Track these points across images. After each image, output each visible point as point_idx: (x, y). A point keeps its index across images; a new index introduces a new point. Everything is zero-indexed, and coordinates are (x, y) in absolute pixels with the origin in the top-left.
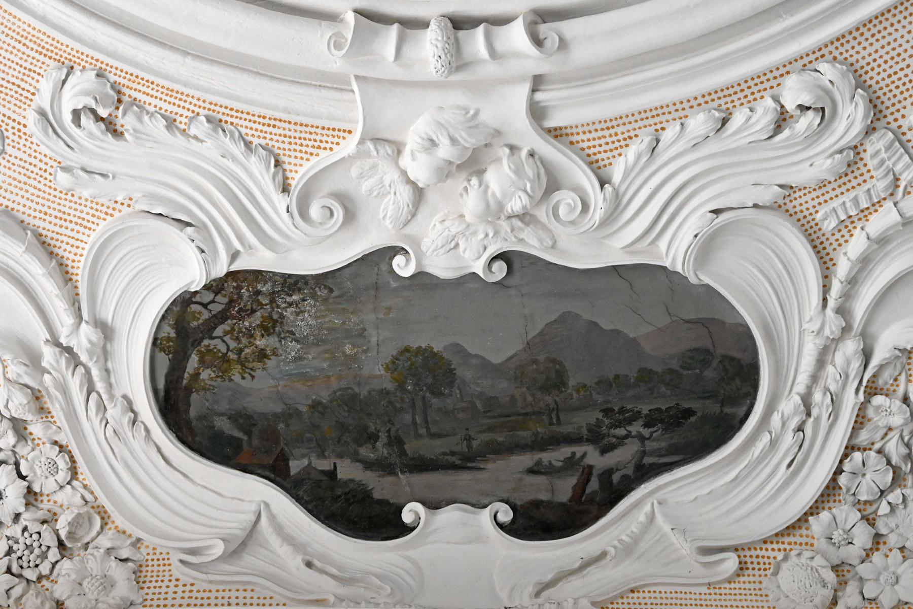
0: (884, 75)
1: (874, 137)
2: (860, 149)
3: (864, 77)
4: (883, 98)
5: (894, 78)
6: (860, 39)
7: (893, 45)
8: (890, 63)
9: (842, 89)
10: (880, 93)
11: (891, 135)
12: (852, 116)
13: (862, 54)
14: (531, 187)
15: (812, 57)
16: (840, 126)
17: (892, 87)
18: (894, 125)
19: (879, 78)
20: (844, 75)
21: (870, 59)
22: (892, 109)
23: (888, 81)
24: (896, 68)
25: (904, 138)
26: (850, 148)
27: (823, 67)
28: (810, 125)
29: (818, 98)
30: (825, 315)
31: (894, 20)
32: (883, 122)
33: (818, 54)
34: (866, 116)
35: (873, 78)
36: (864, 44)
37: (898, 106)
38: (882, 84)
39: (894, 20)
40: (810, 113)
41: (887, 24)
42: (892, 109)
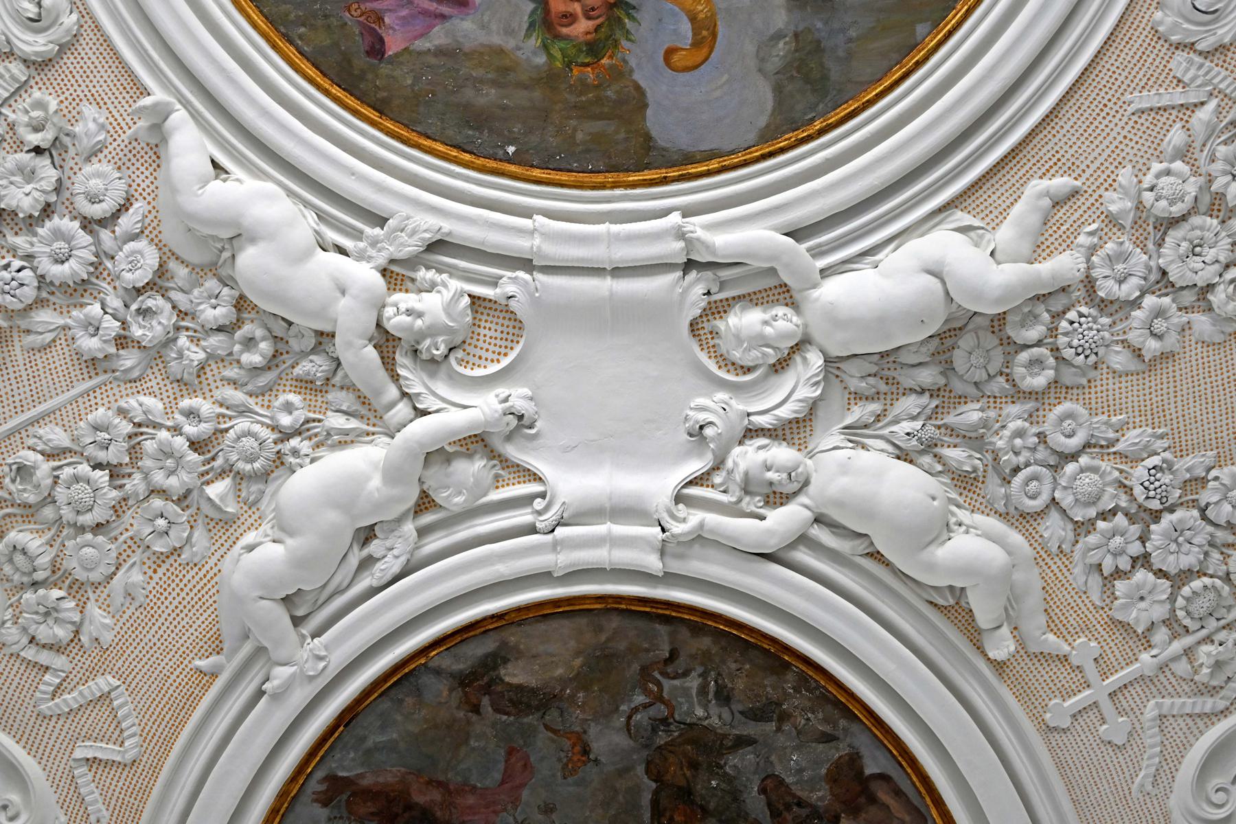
0: (71, 67)
1: (22, 66)
2: (11, 58)
3: (69, 53)
4: (53, 71)
5: (70, 76)
6: (98, 44)
7: (95, 71)
8: (81, 71)
9: (56, 33)
10: (57, 67)
11: (24, 79)
12: (35, 44)
13: (87, 47)
14: (145, 107)
15: (82, 8)
16: (29, 37)
17: (63, 76)
18: (32, 82)
19: (69, 64)
20: (68, 31)
21: (83, 55)
22: (45, 79)
23: (67, 72)
24: (78, 77)
25: (22, 92)
26: (12, 49)
27: (74, 17)
28: (26, 10)
29: (49, 11)
30: (671, 643)
31: (114, 68)
32: (34, 73)
33: (84, 13)
34: (36, 54)
35: (69, 59)
36: (94, 48)
37: (48, 83)
38: (64, 68)
39: (114, 68)
40: (36, 10)
41: (110, 63)
42: (45, 79)
